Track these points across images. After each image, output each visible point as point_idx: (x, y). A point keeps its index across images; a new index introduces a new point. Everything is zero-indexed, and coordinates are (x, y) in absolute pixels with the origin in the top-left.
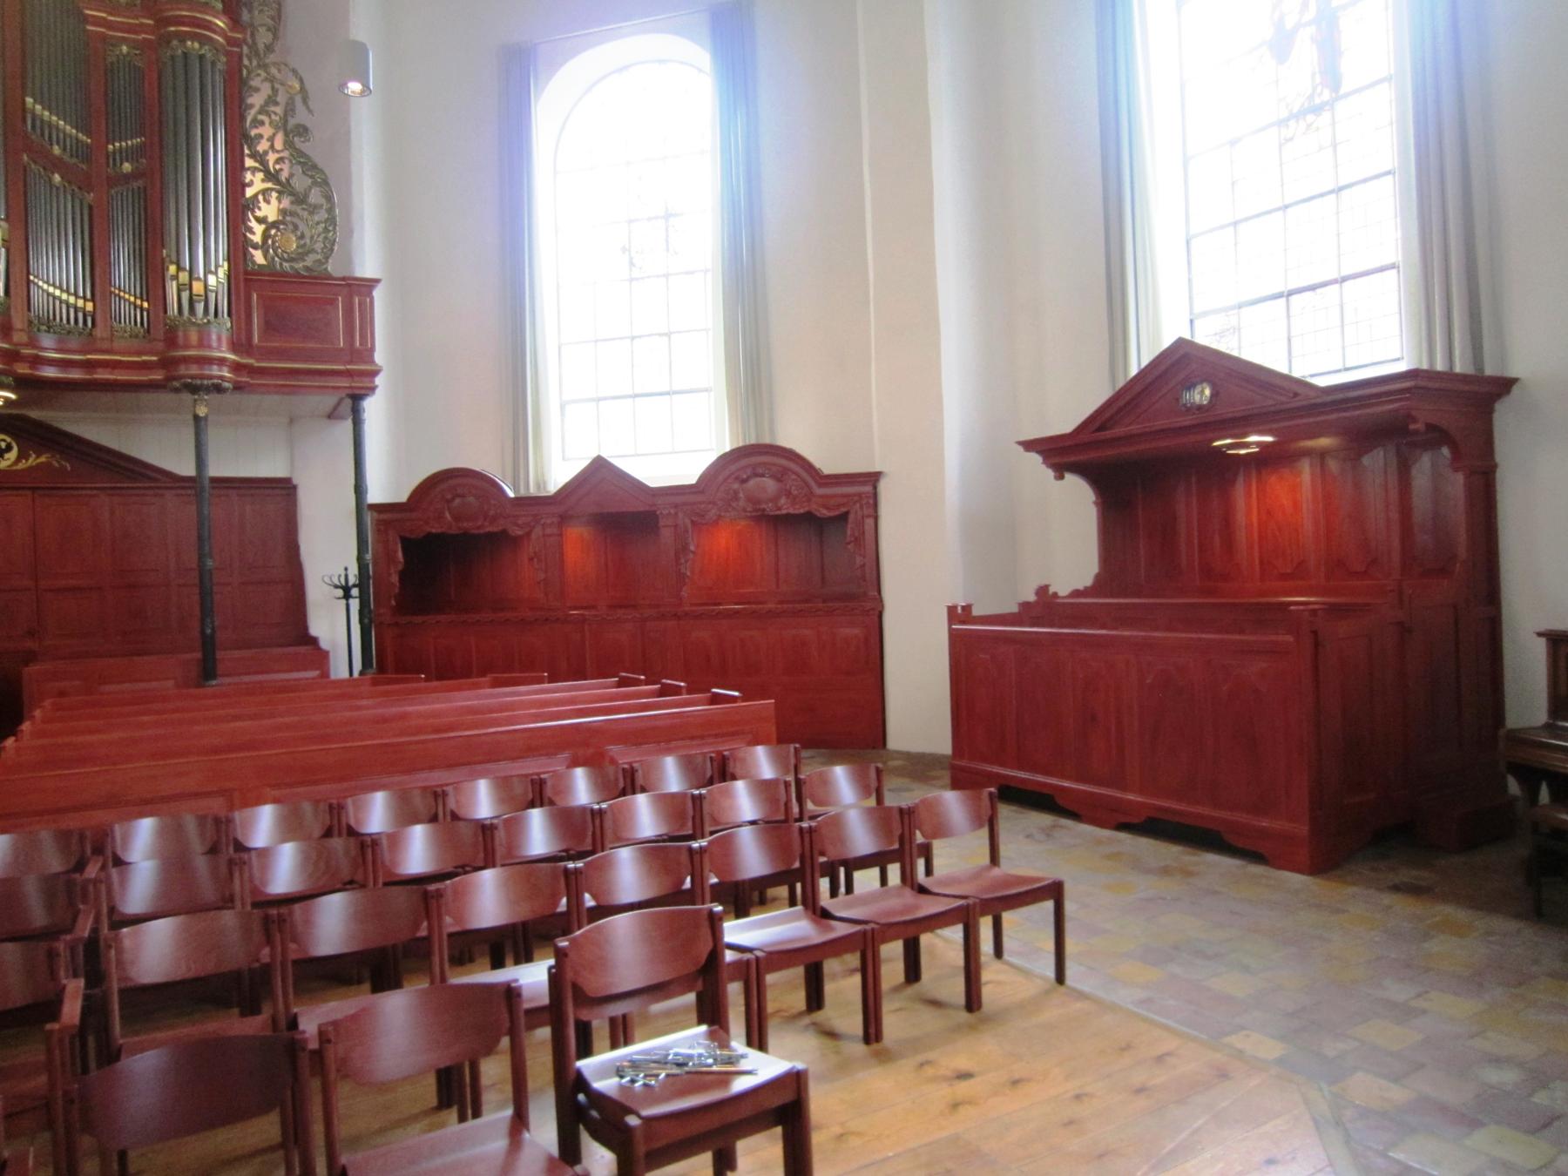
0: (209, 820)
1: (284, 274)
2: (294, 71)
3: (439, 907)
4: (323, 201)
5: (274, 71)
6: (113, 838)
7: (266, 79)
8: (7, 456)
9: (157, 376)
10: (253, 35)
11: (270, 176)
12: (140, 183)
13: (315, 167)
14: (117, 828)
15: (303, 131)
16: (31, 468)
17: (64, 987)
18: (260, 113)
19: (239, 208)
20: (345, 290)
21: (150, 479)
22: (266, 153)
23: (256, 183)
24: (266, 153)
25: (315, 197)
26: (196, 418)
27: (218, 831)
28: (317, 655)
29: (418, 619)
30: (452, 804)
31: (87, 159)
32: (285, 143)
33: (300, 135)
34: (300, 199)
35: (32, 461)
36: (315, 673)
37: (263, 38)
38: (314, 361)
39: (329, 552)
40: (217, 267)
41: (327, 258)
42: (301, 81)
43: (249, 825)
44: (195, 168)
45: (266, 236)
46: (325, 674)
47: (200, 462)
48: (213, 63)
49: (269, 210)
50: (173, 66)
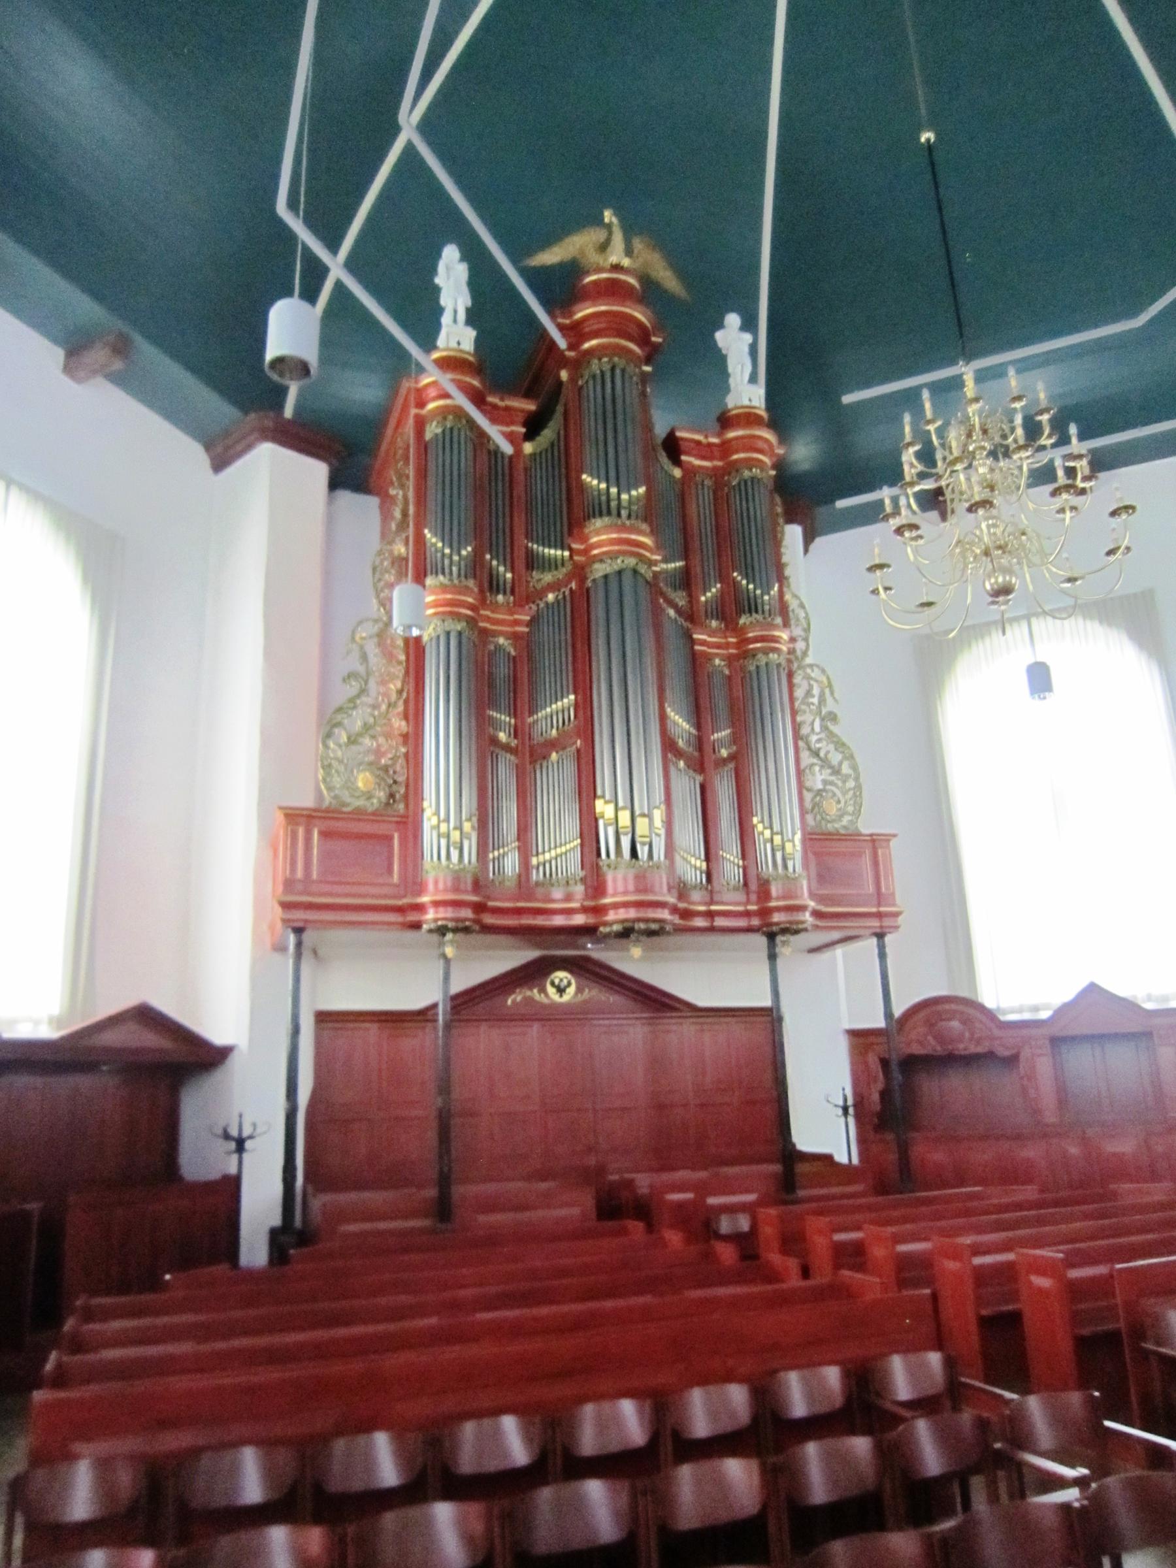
4: (850, 772)
5: (809, 671)
8: (568, 990)
13: (844, 744)
15: (833, 717)
25: (846, 769)
32: (821, 726)
40: (794, 834)
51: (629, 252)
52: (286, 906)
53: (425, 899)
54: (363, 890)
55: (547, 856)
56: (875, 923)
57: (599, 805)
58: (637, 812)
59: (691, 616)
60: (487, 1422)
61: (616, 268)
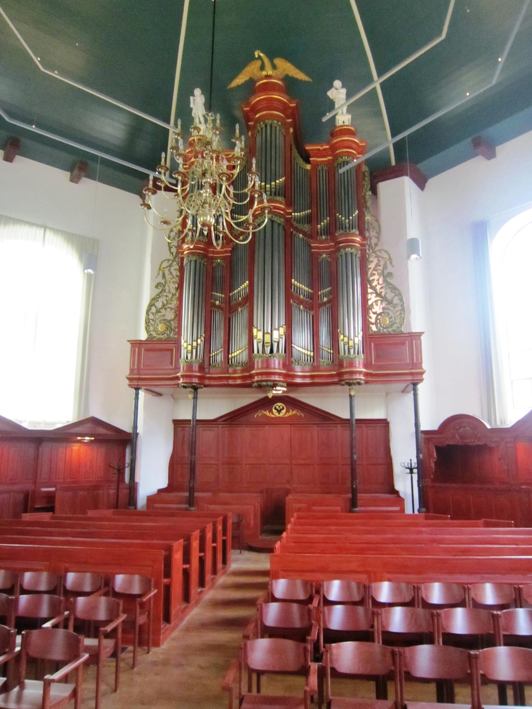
0: (361, 585)
1: (385, 334)
2: (386, 252)
3: (476, 663)
4: (399, 302)
5: (378, 253)
6: (323, 587)
7: (375, 257)
8: (282, 411)
9: (336, 380)
10: (370, 241)
11: (378, 295)
12: (330, 305)
14: (325, 583)
15: (390, 274)
16: (290, 416)
17: (310, 667)
18: (374, 270)
19: (366, 309)
20: (409, 338)
21: (333, 420)
22: (376, 286)
23: (372, 298)
24: (376, 286)
25: (396, 301)
26: (351, 396)
27: (365, 592)
28: (399, 500)
29: (444, 485)
30: (472, 595)
31: (311, 298)
33: (389, 276)
34: (390, 302)
35: (291, 413)
36: (397, 509)
37: (374, 241)
38: (396, 369)
39: (404, 452)
41: (401, 325)
42: (389, 255)
43: (379, 589)
44: (350, 297)
45: (377, 319)
46: (403, 510)
47: (352, 414)
48: (356, 255)
49: (378, 309)
50: (342, 258)
51: (274, 67)
52: (130, 379)
53: (179, 374)
54: (157, 372)
55: (236, 354)
56: (410, 378)
57: (255, 330)
58: (265, 332)
59: (312, 236)
60: (82, 574)
61: (267, 77)
